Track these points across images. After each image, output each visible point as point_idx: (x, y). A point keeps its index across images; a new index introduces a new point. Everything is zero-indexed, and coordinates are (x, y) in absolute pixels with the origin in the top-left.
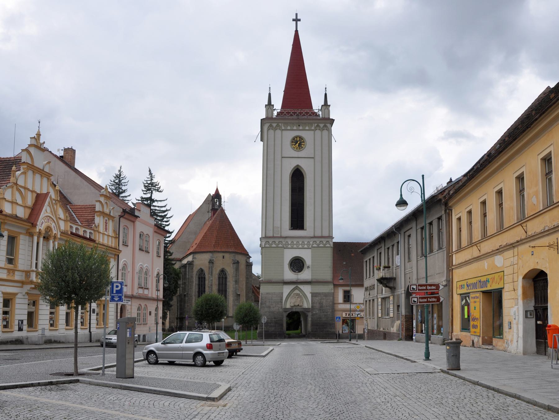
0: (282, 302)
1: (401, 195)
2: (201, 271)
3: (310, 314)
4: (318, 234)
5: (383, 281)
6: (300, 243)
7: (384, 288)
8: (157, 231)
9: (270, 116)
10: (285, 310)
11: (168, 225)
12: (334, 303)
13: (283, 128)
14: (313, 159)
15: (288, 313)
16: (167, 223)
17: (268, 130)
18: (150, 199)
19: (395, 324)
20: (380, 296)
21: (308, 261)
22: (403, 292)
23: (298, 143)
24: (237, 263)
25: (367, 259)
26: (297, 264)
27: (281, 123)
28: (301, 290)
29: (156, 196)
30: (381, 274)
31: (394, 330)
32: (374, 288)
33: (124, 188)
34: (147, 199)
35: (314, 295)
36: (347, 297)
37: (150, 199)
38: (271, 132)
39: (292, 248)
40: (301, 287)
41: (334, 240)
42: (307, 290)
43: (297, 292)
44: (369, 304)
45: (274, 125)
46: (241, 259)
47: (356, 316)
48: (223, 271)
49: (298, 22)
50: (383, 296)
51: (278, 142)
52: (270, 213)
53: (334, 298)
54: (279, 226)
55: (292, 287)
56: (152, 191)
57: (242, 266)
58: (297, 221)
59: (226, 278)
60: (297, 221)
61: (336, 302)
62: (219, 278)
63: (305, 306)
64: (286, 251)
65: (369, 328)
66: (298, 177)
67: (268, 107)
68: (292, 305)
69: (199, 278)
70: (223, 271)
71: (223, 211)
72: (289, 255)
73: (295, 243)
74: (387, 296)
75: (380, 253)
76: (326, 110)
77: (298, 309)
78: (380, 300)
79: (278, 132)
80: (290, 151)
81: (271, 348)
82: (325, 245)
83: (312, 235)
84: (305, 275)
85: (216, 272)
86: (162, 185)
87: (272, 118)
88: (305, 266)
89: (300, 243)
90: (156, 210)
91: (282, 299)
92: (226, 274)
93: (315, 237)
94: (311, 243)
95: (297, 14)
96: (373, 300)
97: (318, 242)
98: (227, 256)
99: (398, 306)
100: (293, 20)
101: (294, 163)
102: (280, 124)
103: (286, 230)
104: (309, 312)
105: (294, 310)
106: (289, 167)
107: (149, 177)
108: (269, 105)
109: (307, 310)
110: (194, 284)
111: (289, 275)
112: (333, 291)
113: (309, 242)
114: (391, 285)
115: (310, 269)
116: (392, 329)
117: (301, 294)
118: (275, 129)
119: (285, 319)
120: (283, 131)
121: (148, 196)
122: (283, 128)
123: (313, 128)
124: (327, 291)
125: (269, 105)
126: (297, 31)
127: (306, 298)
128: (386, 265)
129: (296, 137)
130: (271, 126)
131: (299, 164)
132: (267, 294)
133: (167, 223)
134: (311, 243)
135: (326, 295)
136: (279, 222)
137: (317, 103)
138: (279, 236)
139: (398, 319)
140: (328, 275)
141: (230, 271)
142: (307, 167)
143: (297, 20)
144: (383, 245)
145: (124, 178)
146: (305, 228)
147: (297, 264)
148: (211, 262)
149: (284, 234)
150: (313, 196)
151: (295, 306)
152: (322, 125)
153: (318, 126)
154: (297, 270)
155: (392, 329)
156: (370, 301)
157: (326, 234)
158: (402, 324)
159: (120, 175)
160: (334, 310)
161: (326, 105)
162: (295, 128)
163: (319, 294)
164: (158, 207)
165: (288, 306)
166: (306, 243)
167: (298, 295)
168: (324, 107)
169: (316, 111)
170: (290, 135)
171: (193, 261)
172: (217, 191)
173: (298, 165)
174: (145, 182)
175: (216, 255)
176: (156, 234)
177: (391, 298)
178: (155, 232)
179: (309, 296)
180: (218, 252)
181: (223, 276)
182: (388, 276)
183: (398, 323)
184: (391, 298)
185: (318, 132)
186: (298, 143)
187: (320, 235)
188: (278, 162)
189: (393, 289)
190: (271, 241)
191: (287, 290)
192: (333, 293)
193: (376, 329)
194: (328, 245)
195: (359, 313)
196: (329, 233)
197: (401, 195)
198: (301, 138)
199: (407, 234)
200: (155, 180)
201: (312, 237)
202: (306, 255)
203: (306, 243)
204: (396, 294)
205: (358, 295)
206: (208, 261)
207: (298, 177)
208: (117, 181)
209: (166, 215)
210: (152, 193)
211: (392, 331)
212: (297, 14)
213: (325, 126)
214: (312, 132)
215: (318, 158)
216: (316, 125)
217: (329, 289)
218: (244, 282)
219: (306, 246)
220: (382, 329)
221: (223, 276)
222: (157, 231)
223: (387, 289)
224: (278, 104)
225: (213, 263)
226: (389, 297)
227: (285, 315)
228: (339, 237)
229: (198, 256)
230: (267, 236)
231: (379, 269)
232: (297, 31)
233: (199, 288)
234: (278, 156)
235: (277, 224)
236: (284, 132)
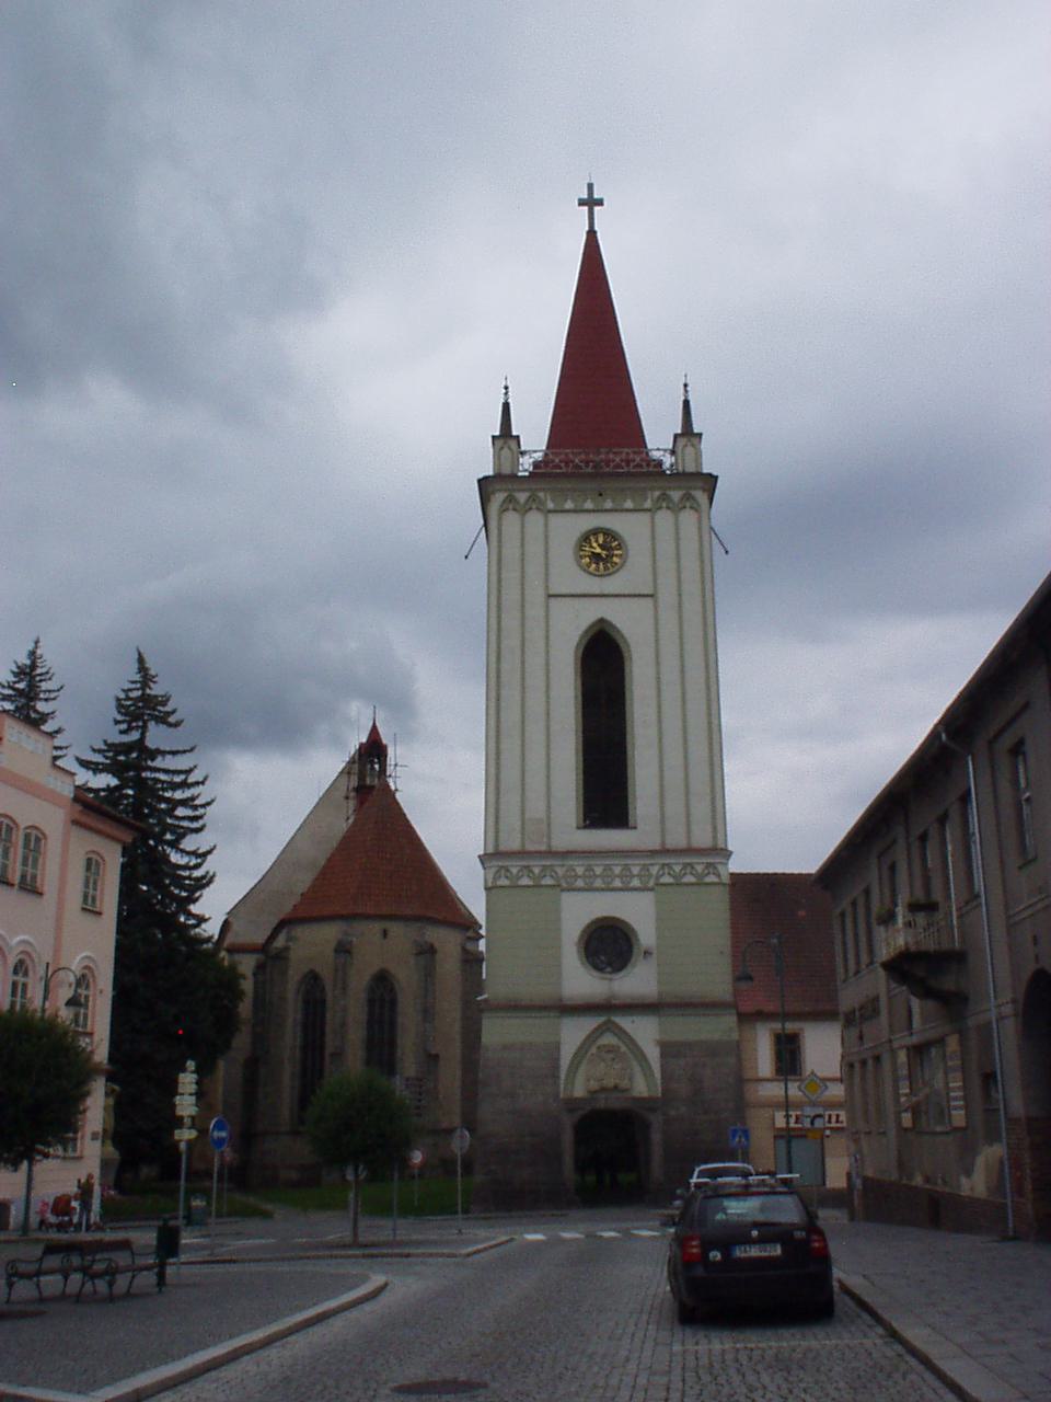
0: (556, 1077)
1: (523, 526)
2: (313, 979)
3: (656, 1120)
4: (676, 839)
5: (903, 967)
6: (617, 870)
7: (916, 1003)
8: (84, 819)
9: (506, 470)
10: (571, 1104)
11: (198, 830)
12: (741, 1081)
13: (550, 505)
14: (649, 600)
15: (581, 1113)
16: (195, 825)
17: (503, 510)
18: (140, 744)
19: (980, 1161)
20: (904, 1039)
21: (646, 934)
22: (1008, 1010)
23: (603, 552)
24: (428, 952)
25: (845, 904)
26: (609, 944)
27: (543, 490)
28: (621, 1033)
29: (156, 736)
30: (895, 939)
31: (975, 1184)
32: (876, 1012)
33: (41, 706)
34: (126, 748)
35: (668, 1050)
36: (788, 1057)
37: (140, 744)
38: (512, 518)
39: (590, 889)
40: (625, 1022)
41: (736, 865)
42: (645, 1032)
43: (608, 1039)
44: (863, 1078)
45: (522, 497)
46: (447, 942)
47: (807, 1123)
48: (382, 980)
49: (596, 209)
50: (915, 1040)
51: (535, 549)
52: (511, 775)
53: (739, 1060)
54: (541, 814)
55: (589, 1024)
56: (145, 723)
57: (449, 964)
58: (605, 791)
59: (393, 1003)
60: (605, 791)
61: (748, 1074)
62: (371, 1002)
63: (641, 1088)
64: (568, 900)
65: (869, 1173)
66: (603, 659)
67: (499, 443)
68: (594, 1085)
69: (306, 1002)
70: (382, 980)
71: (389, 795)
72: (578, 912)
73: (598, 871)
74: (931, 1035)
75: (893, 868)
76: (690, 450)
77: (615, 1103)
78: (902, 1056)
79: (535, 519)
80: (569, 574)
81: (377, 1280)
82: (700, 876)
83: (655, 844)
84: (638, 981)
85: (359, 981)
86: (179, 704)
87: (514, 477)
88: (635, 950)
89: (617, 870)
90: (157, 781)
91: (556, 1066)
92: (392, 990)
93: (665, 851)
94: (654, 870)
95: (590, 187)
96: (877, 1059)
97: (677, 869)
98: (397, 929)
99: (989, 1078)
100: (582, 203)
101: (589, 613)
102: (541, 495)
103: (568, 830)
104: (653, 1110)
105: (601, 1104)
106: (571, 626)
107: (137, 677)
108: (506, 436)
109: (649, 1104)
110: (290, 1021)
111: (579, 981)
112: (735, 1036)
113: (645, 868)
114: (948, 983)
115: (653, 960)
116: (963, 1180)
117: (624, 1049)
118: (524, 511)
119: (568, 1138)
120: (552, 517)
121: (135, 736)
122: (550, 505)
123: (648, 504)
124: (716, 1036)
125: (506, 436)
126: (592, 234)
127: (643, 1061)
128: (920, 895)
129: (595, 532)
130: (510, 499)
131: (608, 617)
132: (505, 1047)
133: (195, 825)
134: (654, 870)
135: (712, 1050)
136: (542, 805)
137: (658, 433)
138: (543, 848)
139: (992, 1136)
140: (716, 980)
141: (406, 977)
142: (631, 623)
143: (591, 202)
144: (899, 830)
145: (47, 676)
146: (631, 823)
147: (609, 944)
148: (343, 949)
149: (560, 843)
150: (654, 717)
151: (603, 1089)
152: (676, 495)
153: (664, 497)
154: (610, 964)
155: (963, 1180)
156: (864, 1063)
157: (702, 839)
158: (1016, 1164)
159: (33, 666)
160: (741, 1106)
161: (688, 433)
162: (589, 505)
163: (688, 1045)
164: (166, 771)
165: (579, 1091)
166: (635, 870)
167: (611, 1049)
168: (682, 442)
169: (656, 455)
170: (569, 527)
171: (287, 949)
172: (374, 729)
173: (602, 621)
174: (122, 696)
175: (361, 927)
176: (76, 832)
177: (953, 1043)
178: (75, 822)
179: (653, 1054)
180: (368, 917)
181: (382, 990)
182: (930, 945)
183: (991, 1154)
184: (953, 1043)
185: (664, 518)
186: (603, 552)
187: (682, 844)
188: (535, 611)
189: (953, 1004)
190: (514, 866)
191: (573, 1033)
192: (738, 1044)
193: (894, 1176)
194: (712, 879)
195: (820, 1111)
196: (715, 838)
197: (523, 526)
198: (608, 533)
199: (1008, 740)
200: (156, 690)
201: (653, 853)
202: (638, 912)
203: (635, 870)
204: (971, 1022)
205: (823, 1049)
206: (333, 945)
207: (603, 659)
208: (21, 686)
209: (193, 799)
210: (144, 729)
211: (965, 1191)
212: (590, 187)
213: (688, 497)
214: (644, 518)
215: (667, 595)
216: (657, 493)
217: (720, 1028)
218: (458, 1015)
219: (636, 883)
220: (918, 1180)
221: (382, 990)
222: (84, 819)
223: (931, 1004)
224: (534, 432)
225: (348, 952)
226: (941, 1041)
227: (568, 1123)
228: (748, 857)
229: (302, 932)
230: (502, 848)
231: (888, 918)
232: (592, 234)
233: (574, 1076)
234: (536, 594)
235: (536, 808)
236: (555, 519)
